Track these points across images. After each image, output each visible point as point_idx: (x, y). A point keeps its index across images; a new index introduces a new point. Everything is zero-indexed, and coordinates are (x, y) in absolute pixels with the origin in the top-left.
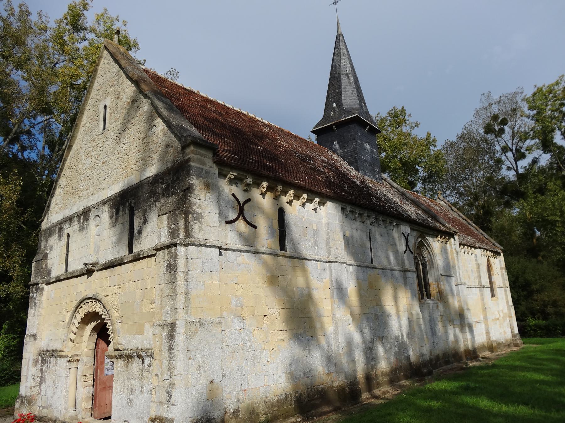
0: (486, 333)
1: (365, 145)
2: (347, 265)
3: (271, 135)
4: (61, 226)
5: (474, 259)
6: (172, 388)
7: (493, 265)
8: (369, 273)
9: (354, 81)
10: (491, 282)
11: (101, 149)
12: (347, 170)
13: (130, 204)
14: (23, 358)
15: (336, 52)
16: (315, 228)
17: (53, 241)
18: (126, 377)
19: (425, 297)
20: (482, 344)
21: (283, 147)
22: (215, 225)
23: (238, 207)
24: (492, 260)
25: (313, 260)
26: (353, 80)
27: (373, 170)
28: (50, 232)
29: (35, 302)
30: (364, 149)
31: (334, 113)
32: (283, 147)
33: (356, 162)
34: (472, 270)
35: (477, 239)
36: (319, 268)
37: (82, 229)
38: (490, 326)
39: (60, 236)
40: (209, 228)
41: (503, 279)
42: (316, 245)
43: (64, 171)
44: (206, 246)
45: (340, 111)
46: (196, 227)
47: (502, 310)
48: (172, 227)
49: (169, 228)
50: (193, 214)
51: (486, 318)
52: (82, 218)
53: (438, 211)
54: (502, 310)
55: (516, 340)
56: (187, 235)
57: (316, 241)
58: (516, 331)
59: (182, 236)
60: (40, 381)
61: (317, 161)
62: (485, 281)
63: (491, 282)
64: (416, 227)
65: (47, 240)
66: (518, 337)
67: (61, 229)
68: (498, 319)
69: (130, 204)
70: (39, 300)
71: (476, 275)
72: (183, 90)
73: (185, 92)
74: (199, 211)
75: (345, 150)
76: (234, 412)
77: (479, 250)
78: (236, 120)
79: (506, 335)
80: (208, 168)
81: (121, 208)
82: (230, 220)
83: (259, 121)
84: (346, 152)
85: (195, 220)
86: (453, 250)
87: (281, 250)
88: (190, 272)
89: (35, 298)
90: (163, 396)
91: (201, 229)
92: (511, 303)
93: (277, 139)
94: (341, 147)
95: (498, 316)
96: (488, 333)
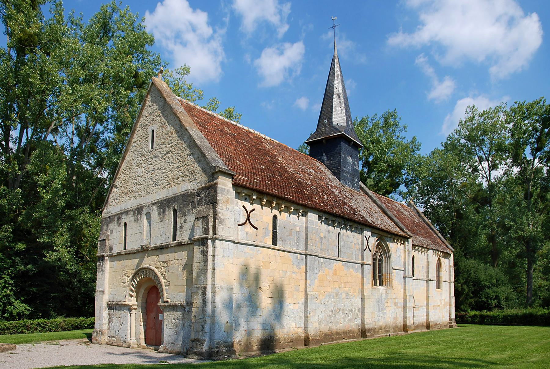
0: (427, 315)
1: (348, 158)
2: (319, 257)
3: (271, 152)
4: (119, 216)
5: (426, 258)
6: (205, 323)
7: (442, 263)
8: (335, 264)
9: (344, 101)
10: (438, 277)
11: (150, 163)
12: (330, 180)
13: (174, 207)
14: (96, 305)
15: (331, 73)
16: (298, 230)
17: (113, 226)
18: (173, 318)
19: (378, 284)
20: (422, 323)
21: (280, 163)
22: (232, 227)
23: (246, 215)
24: (442, 259)
25: (294, 253)
26: (343, 100)
27: (353, 180)
28: (110, 219)
29: (102, 269)
30: (346, 162)
31: (325, 129)
32: (280, 163)
33: (339, 173)
34: (423, 267)
35: (433, 242)
36: (299, 258)
37: (136, 220)
38: (430, 310)
39: (119, 224)
40: (228, 229)
41: (450, 275)
42: (298, 242)
43: (119, 174)
44: (226, 241)
45: (330, 128)
46: (219, 228)
47: (444, 300)
48: (205, 227)
49: (203, 227)
50: (218, 219)
51: (428, 304)
52: (136, 212)
53: (405, 215)
54: (444, 300)
55: (451, 323)
56: (214, 233)
57: (298, 239)
58: (453, 316)
59: (211, 233)
60: (109, 321)
61: (306, 175)
62: (433, 275)
63: (438, 277)
64: (377, 232)
65: (107, 226)
66: (454, 321)
67: (119, 218)
68: (439, 306)
69: (174, 207)
70: (105, 267)
71: (425, 270)
72: (207, 116)
73: (208, 117)
74: (222, 217)
75: (332, 162)
76: (239, 342)
77: (431, 251)
78: (245, 140)
79: (444, 319)
80: (228, 188)
81: (167, 209)
82: (241, 223)
83: (262, 138)
84: (332, 164)
85: (220, 223)
86: (406, 250)
87: (273, 245)
88: (216, 256)
89: (102, 266)
90: (200, 329)
91: (223, 229)
92: (453, 294)
93: (276, 155)
94: (329, 159)
95: (439, 304)
96: (428, 315)
